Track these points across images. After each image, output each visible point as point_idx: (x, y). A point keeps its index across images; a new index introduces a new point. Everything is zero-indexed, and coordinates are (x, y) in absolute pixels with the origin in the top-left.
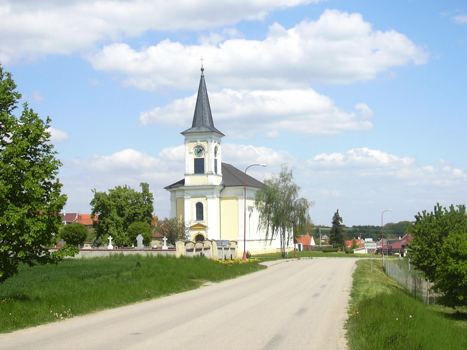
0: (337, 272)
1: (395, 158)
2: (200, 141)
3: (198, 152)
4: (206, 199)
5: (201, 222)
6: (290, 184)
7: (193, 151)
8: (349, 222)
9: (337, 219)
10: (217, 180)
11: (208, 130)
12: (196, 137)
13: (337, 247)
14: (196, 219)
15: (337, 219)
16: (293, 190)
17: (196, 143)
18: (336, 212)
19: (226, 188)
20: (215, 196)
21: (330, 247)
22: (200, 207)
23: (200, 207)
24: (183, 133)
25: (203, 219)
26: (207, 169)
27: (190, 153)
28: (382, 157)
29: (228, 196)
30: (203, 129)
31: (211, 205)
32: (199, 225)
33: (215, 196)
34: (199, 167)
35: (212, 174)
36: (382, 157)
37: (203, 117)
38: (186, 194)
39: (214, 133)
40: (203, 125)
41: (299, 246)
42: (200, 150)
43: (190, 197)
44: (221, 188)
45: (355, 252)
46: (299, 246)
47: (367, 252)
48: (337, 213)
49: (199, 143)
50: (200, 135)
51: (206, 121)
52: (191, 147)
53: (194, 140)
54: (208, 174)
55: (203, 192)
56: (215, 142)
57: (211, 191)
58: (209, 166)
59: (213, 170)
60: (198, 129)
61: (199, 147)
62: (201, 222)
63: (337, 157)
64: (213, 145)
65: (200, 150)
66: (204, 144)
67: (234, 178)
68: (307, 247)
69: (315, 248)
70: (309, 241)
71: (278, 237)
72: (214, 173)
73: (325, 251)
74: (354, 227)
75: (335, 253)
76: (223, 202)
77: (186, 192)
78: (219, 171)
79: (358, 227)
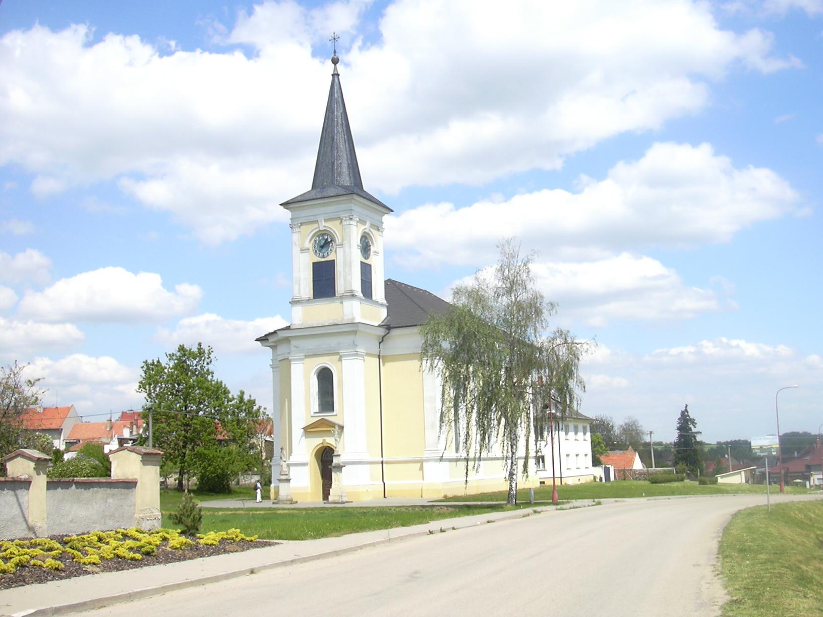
0: (694, 520)
1: (768, 349)
2: (326, 220)
3: (322, 247)
4: (340, 360)
5: (328, 416)
6: (523, 297)
7: (309, 244)
8: (710, 432)
9: (685, 423)
10: (375, 314)
11: (342, 192)
12: (316, 211)
13: (683, 471)
14: (317, 409)
15: (685, 423)
16: (531, 310)
17: (316, 226)
18: (683, 409)
19: (394, 332)
20: (361, 350)
21: (671, 472)
22: (325, 377)
23: (325, 377)
24: (286, 205)
25: (333, 410)
26: (340, 286)
27: (303, 250)
28: (750, 349)
29: (398, 352)
30: (332, 191)
31: (354, 375)
32: (323, 423)
33: (361, 350)
34: (324, 281)
35: (353, 296)
36: (750, 349)
37: (333, 164)
38: (293, 349)
39: (355, 197)
40: (333, 183)
41: (607, 471)
42: (325, 242)
43: (302, 355)
44: (382, 332)
45: (720, 480)
46: (607, 471)
47: (744, 481)
48: (686, 410)
49: (323, 225)
50: (323, 205)
51: (340, 174)
52: (304, 238)
53: (313, 219)
54: (342, 297)
55: (332, 342)
56: (362, 222)
57: (348, 339)
58: (348, 277)
59: (357, 287)
60: (321, 192)
61: (323, 235)
62: (328, 416)
63: (687, 351)
64: (355, 232)
65: (325, 242)
66: (334, 227)
67: (408, 306)
68: (624, 474)
69: (640, 474)
70: (631, 461)
71: (497, 444)
72: (360, 294)
73: (655, 482)
74: (719, 443)
75: (675, 484)
76: (387, 368)
77: (293, 343)
78: (379, 291)
79: (724, 443)
